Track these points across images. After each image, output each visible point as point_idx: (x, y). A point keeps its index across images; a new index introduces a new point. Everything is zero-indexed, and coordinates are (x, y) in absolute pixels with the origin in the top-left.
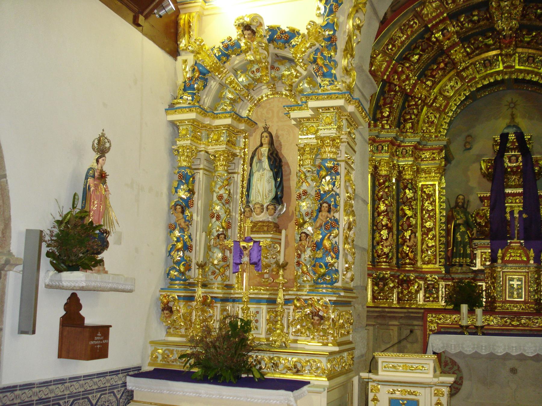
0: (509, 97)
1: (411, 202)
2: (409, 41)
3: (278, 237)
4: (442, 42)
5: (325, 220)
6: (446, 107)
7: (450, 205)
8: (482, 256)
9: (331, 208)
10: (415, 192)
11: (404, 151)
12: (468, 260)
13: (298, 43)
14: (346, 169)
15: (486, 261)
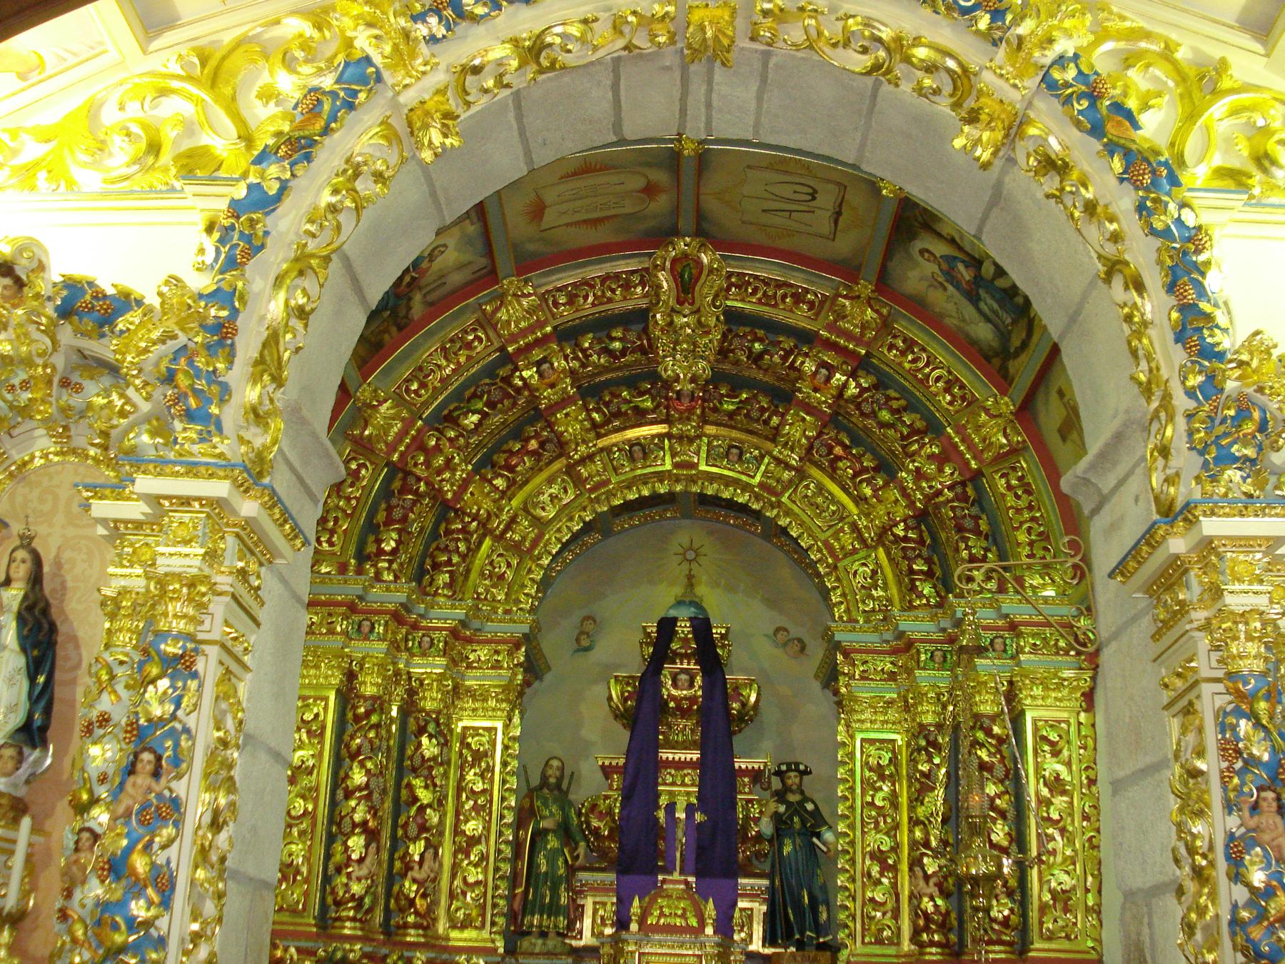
0: (687, 533)
1: (431, 768)
2: (462, 379)
3: (10, 834)
4: (537, 390)
5: (140, 798)
6: (535, 543)
7: (527, 781)
8: (595, 912)
9: (161, 766)
10: (445, 744)
11: (427, 639)
12: (562, 922)
13: (132, 327)
14: (221, 663)
15: (603, 924)
